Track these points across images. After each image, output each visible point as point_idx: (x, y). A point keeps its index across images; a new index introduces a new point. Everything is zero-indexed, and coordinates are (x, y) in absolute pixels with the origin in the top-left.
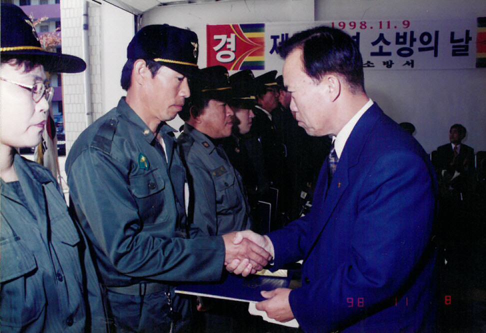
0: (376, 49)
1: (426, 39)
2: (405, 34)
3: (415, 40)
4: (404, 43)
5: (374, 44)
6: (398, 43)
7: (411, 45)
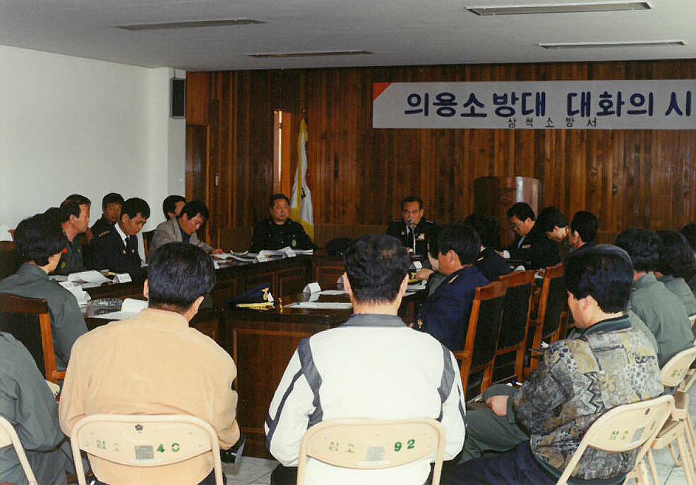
0: (468, 110)
1: (637, 100)
2: (506, 95)
4: (505, 102)
5: (466, 105)
6: (495, 102)
7: (513, 103)
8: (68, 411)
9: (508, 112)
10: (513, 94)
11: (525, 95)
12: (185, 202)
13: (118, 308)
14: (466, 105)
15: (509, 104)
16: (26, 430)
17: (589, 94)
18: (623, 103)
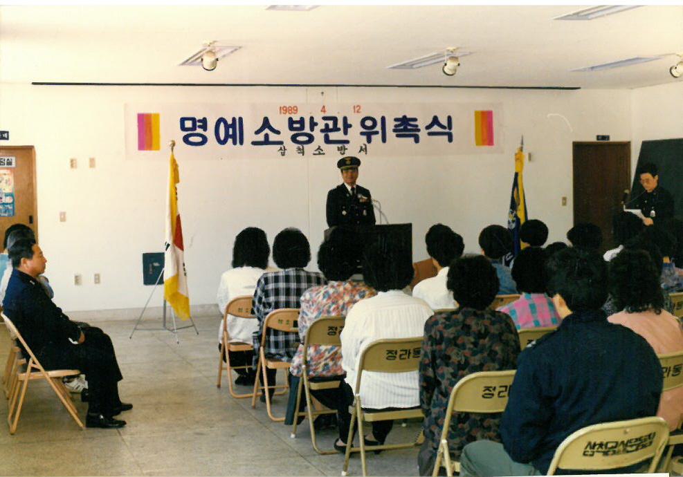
0: (261, 137)
4: (302, 127)
5: (257, 132)
6: (291, 128)
7: (312, 129)
8: (593, 18)
9: (199, 139)
10: (312, 118)
12: (455, 342)
13: (551, 292)
14: (257, 132)
15: (307, 130)
16: (583, 11)
17: (241, 119)
18: (350, 126)
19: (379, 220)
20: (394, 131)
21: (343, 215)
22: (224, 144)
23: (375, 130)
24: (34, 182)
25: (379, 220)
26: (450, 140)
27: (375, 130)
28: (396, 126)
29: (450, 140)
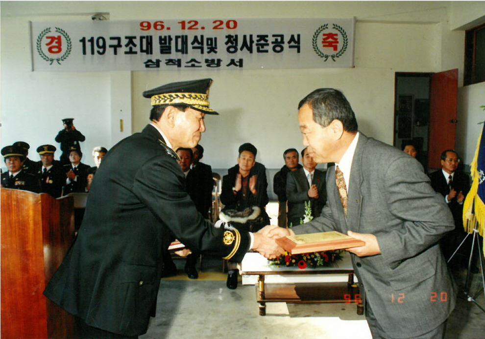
2: (165, 37)
3: (89, 41)
11: (177, 37)
18: (81, 41)
19: (28, 157)
20: (323, 42)
21: (73, 142)
22: (61, 50)
23: (273, 45)
24: (324, 306)
25: (28, 157)
26: (299, 51)
27: (273, 45)
28: (324, 39)
29: (299, 51)
